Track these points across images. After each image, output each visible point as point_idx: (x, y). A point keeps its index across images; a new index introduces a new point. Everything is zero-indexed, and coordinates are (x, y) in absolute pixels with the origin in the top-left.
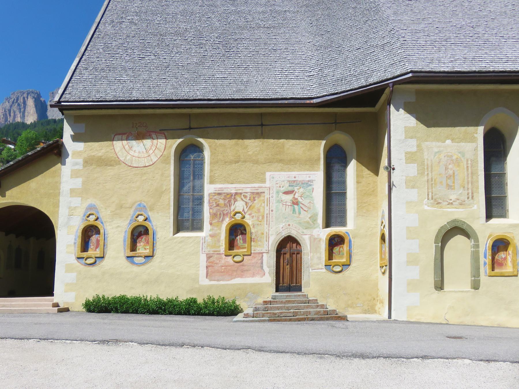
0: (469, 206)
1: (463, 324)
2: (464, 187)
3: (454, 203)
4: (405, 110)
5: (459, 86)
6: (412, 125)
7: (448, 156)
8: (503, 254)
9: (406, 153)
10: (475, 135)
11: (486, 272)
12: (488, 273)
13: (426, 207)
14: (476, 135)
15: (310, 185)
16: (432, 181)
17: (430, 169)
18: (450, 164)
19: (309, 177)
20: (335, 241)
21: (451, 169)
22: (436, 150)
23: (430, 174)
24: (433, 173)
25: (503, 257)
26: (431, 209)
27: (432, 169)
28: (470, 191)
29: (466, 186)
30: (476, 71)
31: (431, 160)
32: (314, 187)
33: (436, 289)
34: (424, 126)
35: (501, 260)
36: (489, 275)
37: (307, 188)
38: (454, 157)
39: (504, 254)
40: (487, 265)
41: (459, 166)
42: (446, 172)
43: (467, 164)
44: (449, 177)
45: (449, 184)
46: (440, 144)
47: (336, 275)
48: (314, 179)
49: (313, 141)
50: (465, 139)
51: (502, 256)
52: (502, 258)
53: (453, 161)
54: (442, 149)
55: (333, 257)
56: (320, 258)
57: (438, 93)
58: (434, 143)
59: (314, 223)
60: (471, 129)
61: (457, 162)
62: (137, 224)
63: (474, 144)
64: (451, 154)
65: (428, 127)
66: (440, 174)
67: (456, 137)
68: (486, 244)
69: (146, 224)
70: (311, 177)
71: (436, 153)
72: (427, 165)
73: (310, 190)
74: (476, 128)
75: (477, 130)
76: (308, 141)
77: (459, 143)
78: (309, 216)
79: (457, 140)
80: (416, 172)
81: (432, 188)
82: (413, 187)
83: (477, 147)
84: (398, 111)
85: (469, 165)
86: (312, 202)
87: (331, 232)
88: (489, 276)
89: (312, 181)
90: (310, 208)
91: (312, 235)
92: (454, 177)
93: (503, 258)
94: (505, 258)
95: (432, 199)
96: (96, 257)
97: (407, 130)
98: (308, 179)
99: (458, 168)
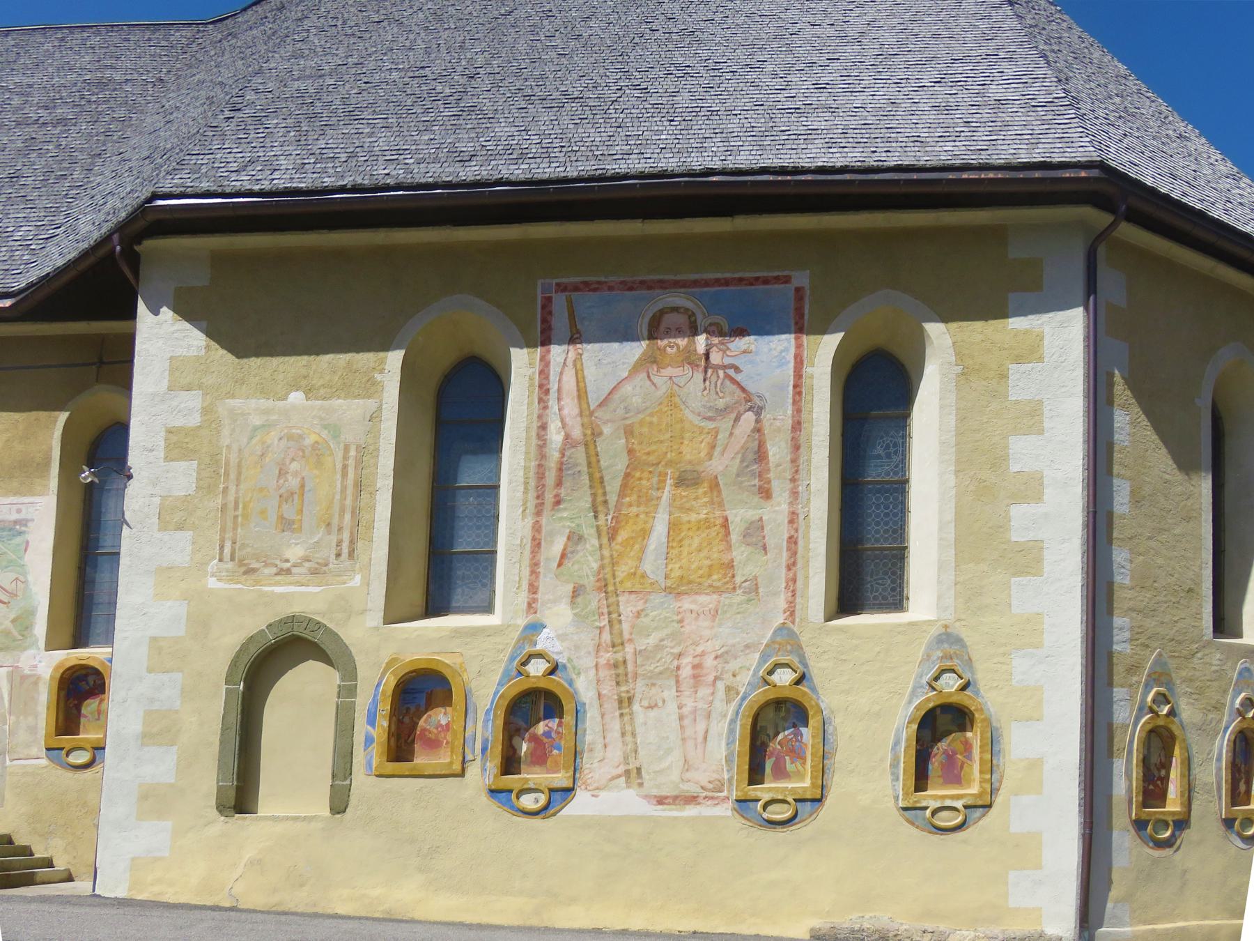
0: (338, 578)
1: (280, 909)
2: (329, 524)
3: (294, 570)
4: (176, 310)
5: (332, 235)
6: (193, 352)
7: (290, 437)
8: (442, 715)
9: (169, 431)
10: (376, 375)
11: (369, 764)
12: (374, 765)
13: (212, 583)
14: (378, 377)
15: (20, 533)
16: (236, 508)
17: (233, 476)
18: (293, 460)
19: (19, 511)
20: (87, 683)
21: (296, 474)
22: (257, 421)
23: (232, 489)
24: (242, 487)
25: (444, 722)
26: (227, 586)
27: (239, 474)
28: (346, 536)
29: (335, 521)
30: (901, 165)
31: (240, 450)
32: (28, 537)
33: (221, 812)
34: (230, 355)
35: (435, 731)
36: (377, 773)
37: (10, 540)
38: (310, 440)
39: (445, 713)
40: (375, 744)
41: (319, 464)
42: (281, 481)
43: (345, 458)
44: (286, 498)
45: (285, 516)
46: (270, 403)
47: (76, 776)
48: (29, 517)
49: (34, 413)
50: (345, 389)
51: (439, 721)
52: (439, 725)
53: (303, 451)
54: (275, 417)
55: (81, 726)
56: (33, 730)
57: (283, 258)
58: (253, 403)
59: (23, 636)
60: (365, 359)
61: (317, 454)
62: (522, 685)
63: (371, 404)
64: (298, 431)
65: (238, 357)
66: (261, 490)
67: (319, 384)
68: (378, 685)
69: (964, 699)
70: (24, 511)
71: (256, 429)
72: (227, 464)
73: (18, 545)
74: (382, 354)
75: (383, 362)
76: (22, 414)
77: (329, 399)
78: (12, 616)
79: (322, 391)
80: (194, 485)
81: (235, 529)
82: (180, 527)
83: (380, 408)
84: (156, 312)
85: (351, 462)
86: (21, 578)
87: (66, 659)
88: (377, 776)
89: (24, 522)
90: (16, 595)
91: (17, 667)
92: (303, 495)
93: (441, 725)
94: (447, 725)
95: (232, 559)
96: (552, 790)
97: (176, 365)
98: (14, 516)
99: (316, 472)
